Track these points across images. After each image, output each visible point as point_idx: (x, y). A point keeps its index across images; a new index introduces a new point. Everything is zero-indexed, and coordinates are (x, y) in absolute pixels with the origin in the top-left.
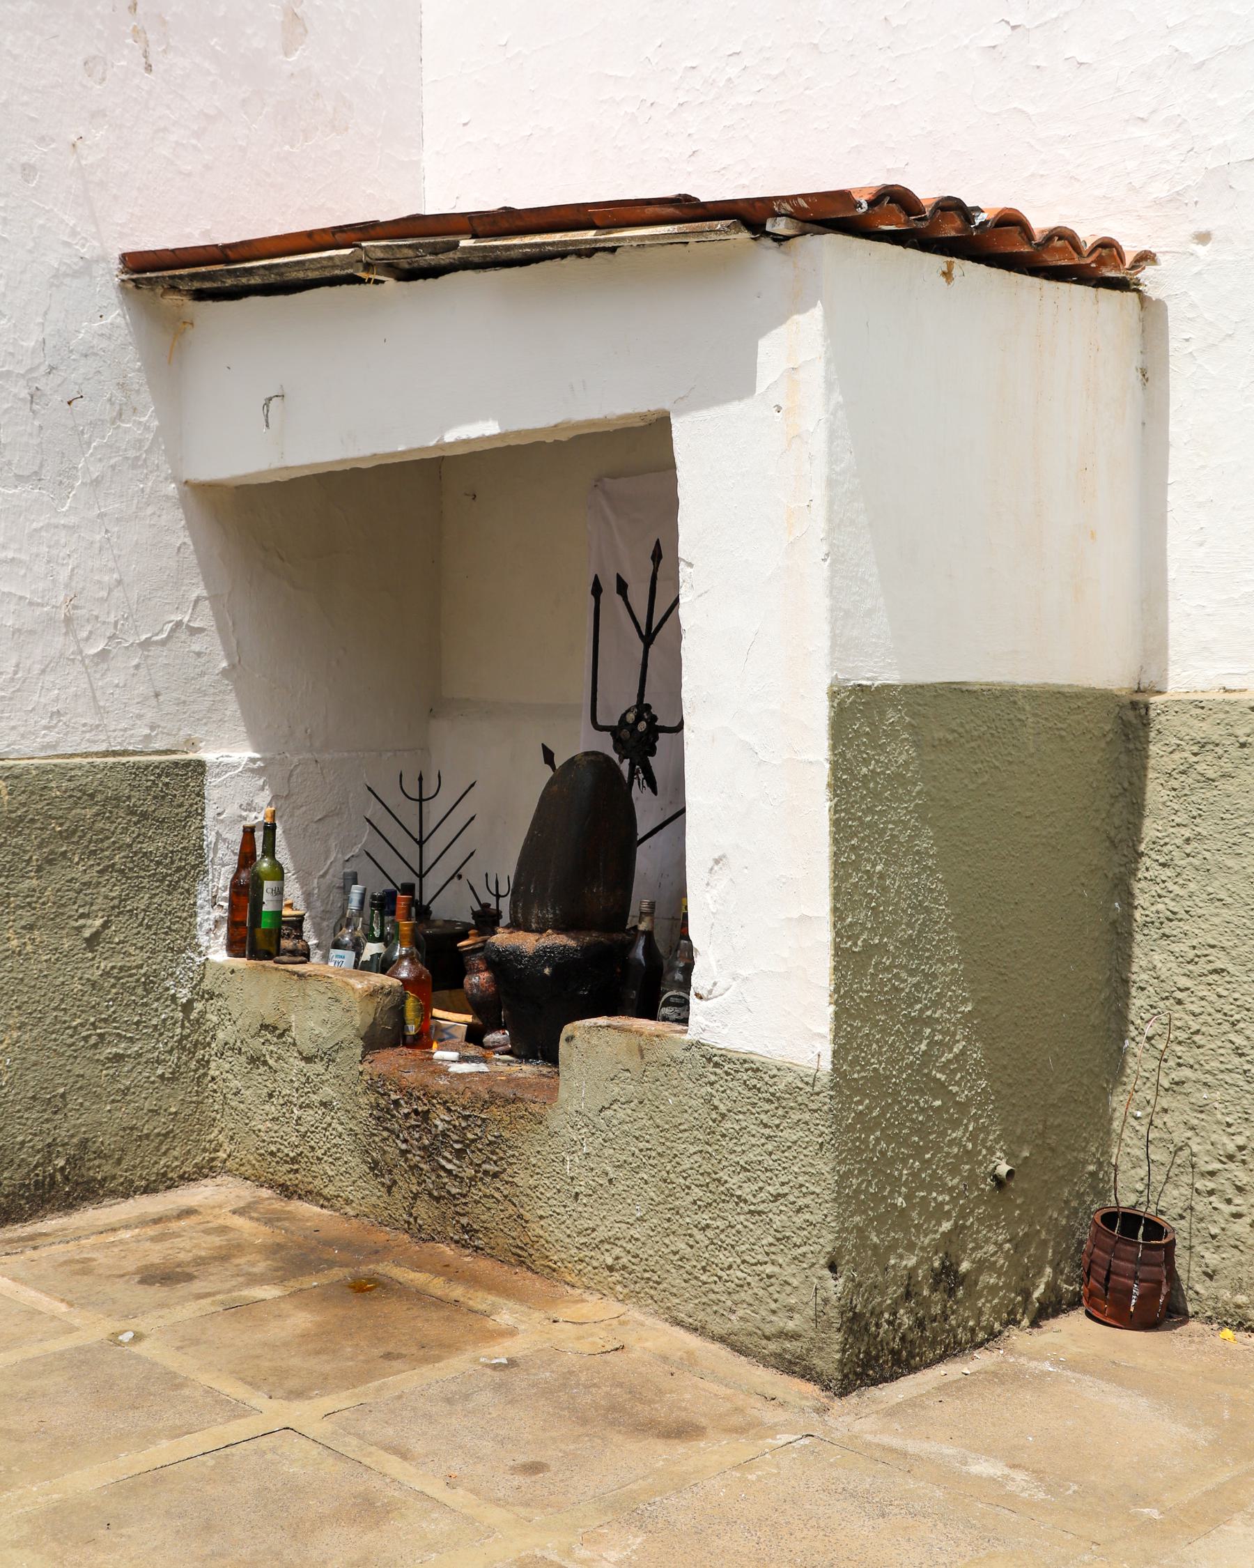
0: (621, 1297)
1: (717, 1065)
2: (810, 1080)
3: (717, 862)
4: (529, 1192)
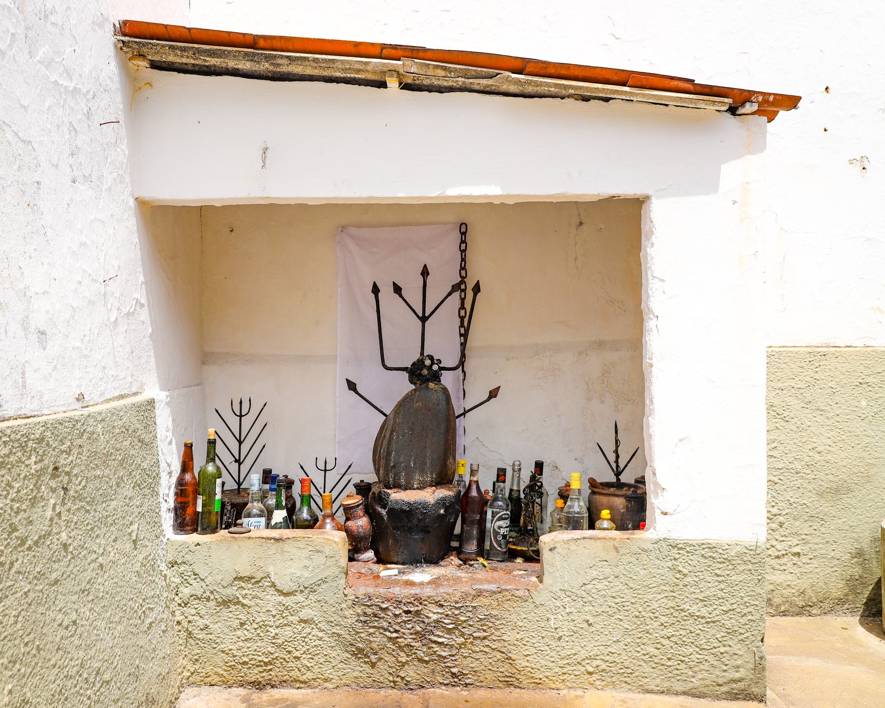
0: (600, 687)
1: (681, 549)
2: (754, 548)
3: (681, 440)
4: (516, 643)
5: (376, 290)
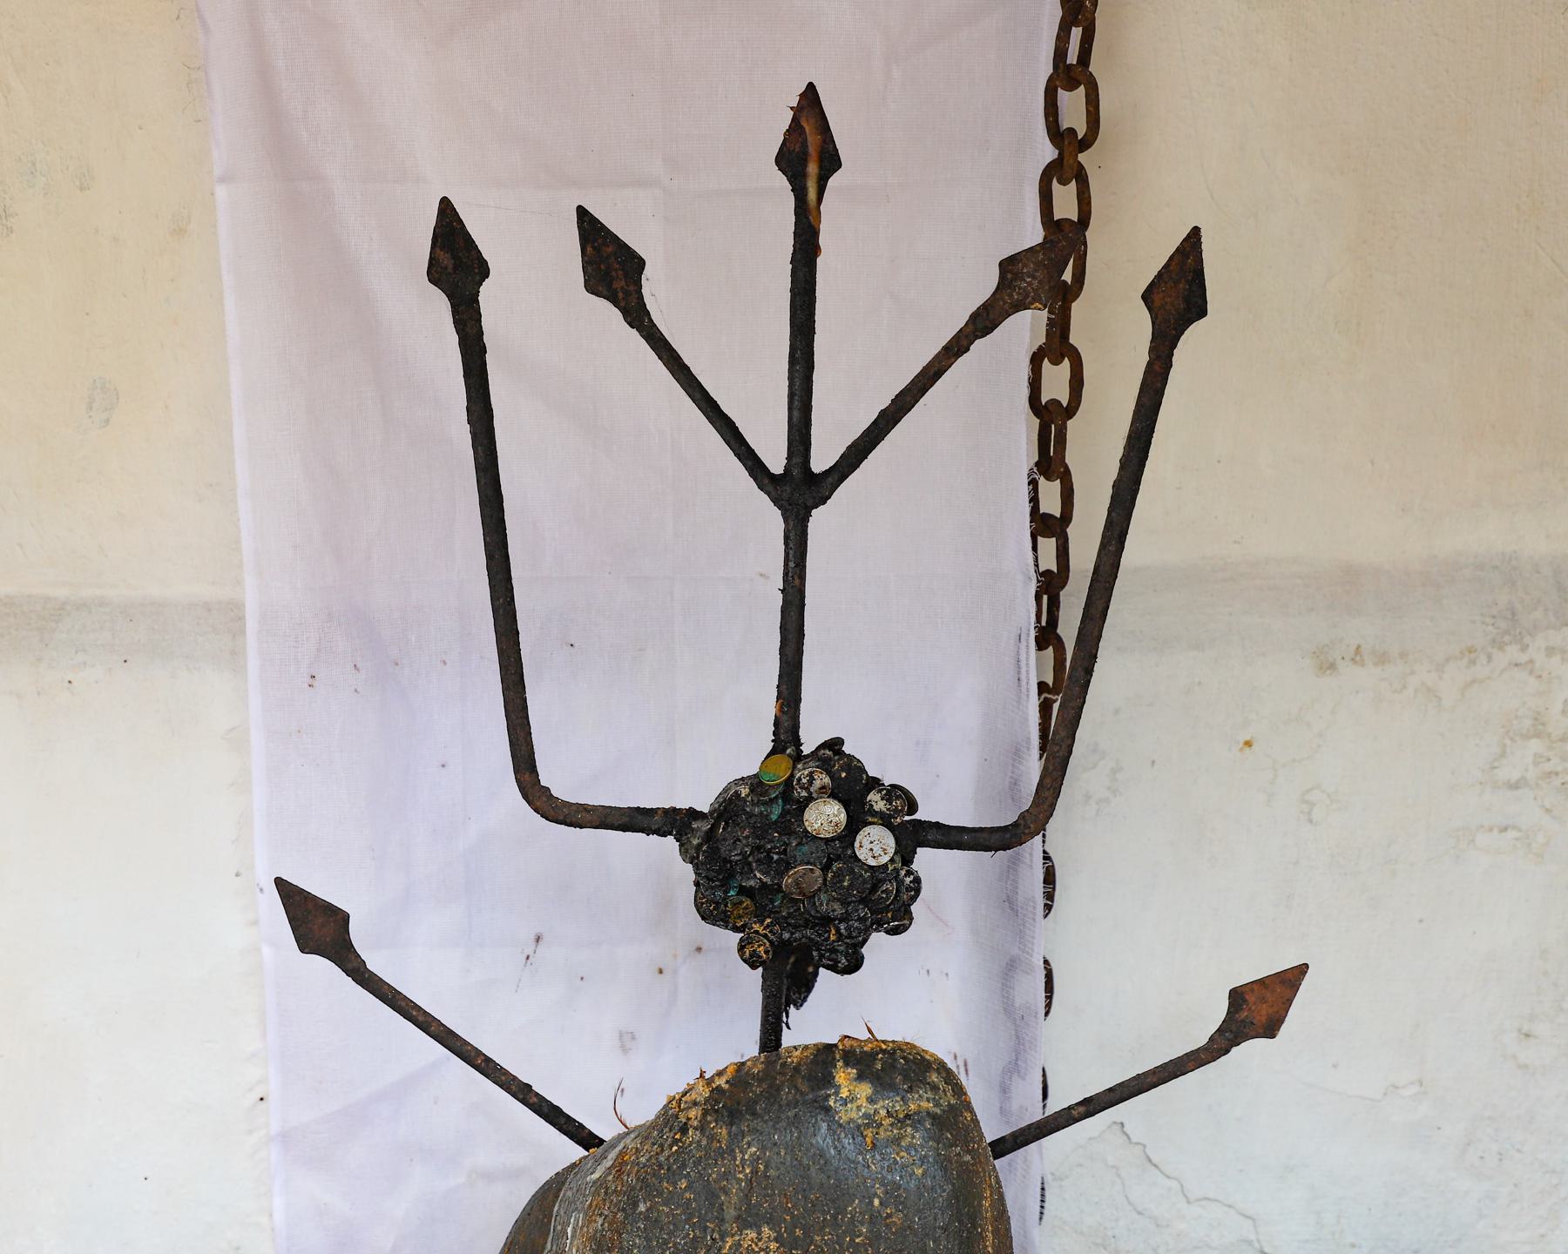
5: (456, 263)
